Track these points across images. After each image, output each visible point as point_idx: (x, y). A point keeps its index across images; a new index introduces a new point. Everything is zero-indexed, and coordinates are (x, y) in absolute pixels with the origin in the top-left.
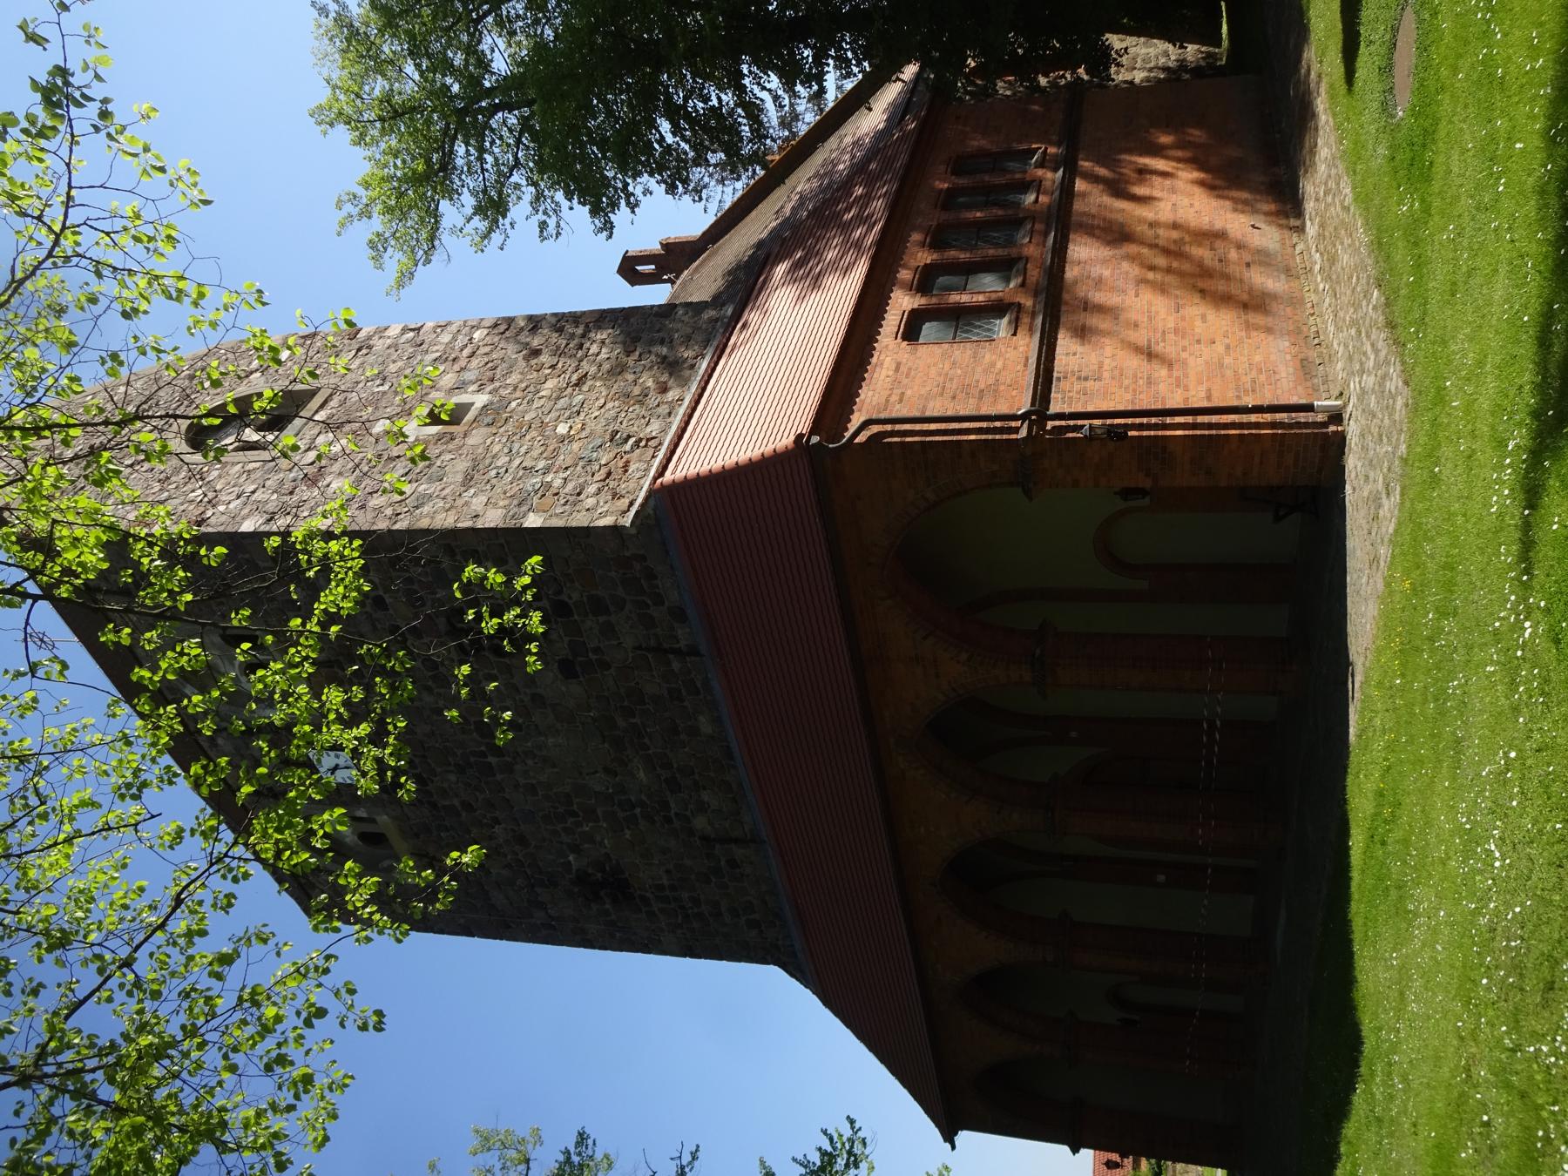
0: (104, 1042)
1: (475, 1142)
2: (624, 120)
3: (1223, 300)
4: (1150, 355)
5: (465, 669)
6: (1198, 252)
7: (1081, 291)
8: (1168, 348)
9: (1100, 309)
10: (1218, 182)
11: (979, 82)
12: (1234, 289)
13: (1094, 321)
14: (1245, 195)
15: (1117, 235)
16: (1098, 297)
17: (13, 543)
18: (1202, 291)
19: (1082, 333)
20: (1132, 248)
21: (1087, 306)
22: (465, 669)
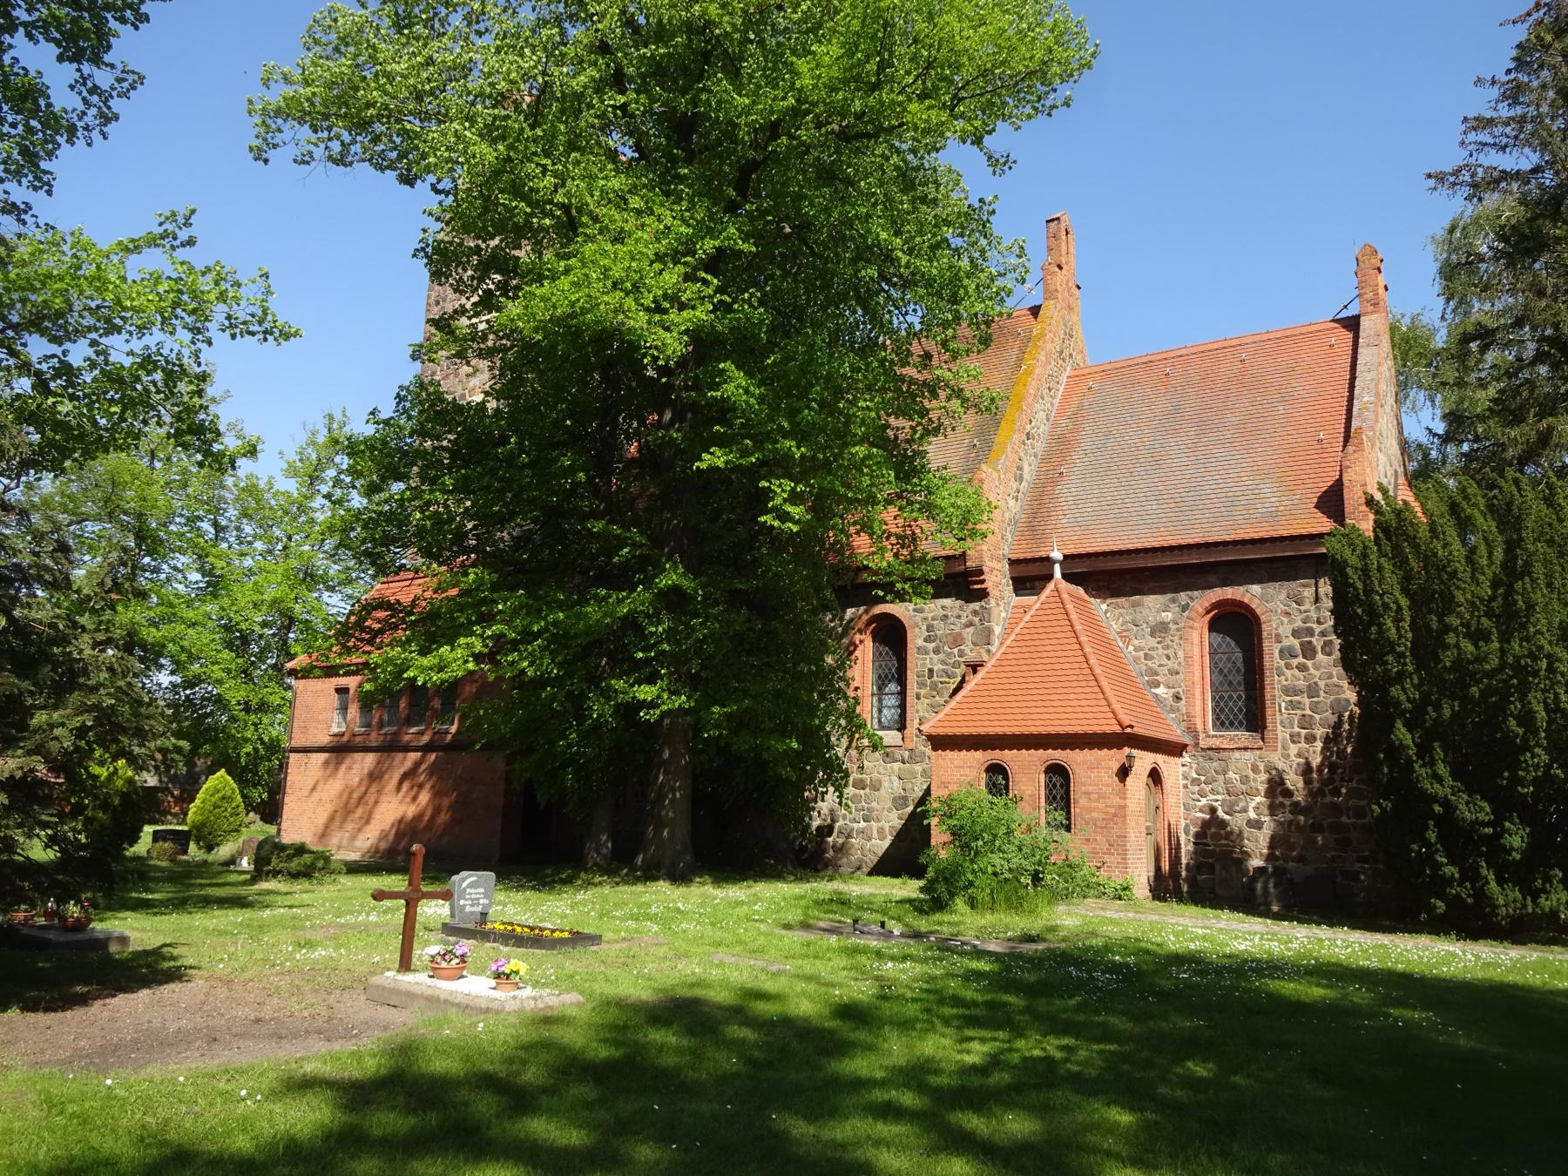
0: (973, 411)
1: (272, 289)
2: (605, 389)
3: (331, 819)
4: (314, 789)
5: (795, 745)
6: (359, 812)
7: (348, 761)
8: (315, 796)
9: (336, 769)
10: (402, 826)
11: (1349, 750)
12: (337, 823)
13: (332, 766)
14: (391, 837)
15: (375, 776)
16: (343, 768)
17: (475, 197)
18: (336, 811)
19: (326, 763)
20: (365, 783)
21: (339, 763)
22: (795, 745)
